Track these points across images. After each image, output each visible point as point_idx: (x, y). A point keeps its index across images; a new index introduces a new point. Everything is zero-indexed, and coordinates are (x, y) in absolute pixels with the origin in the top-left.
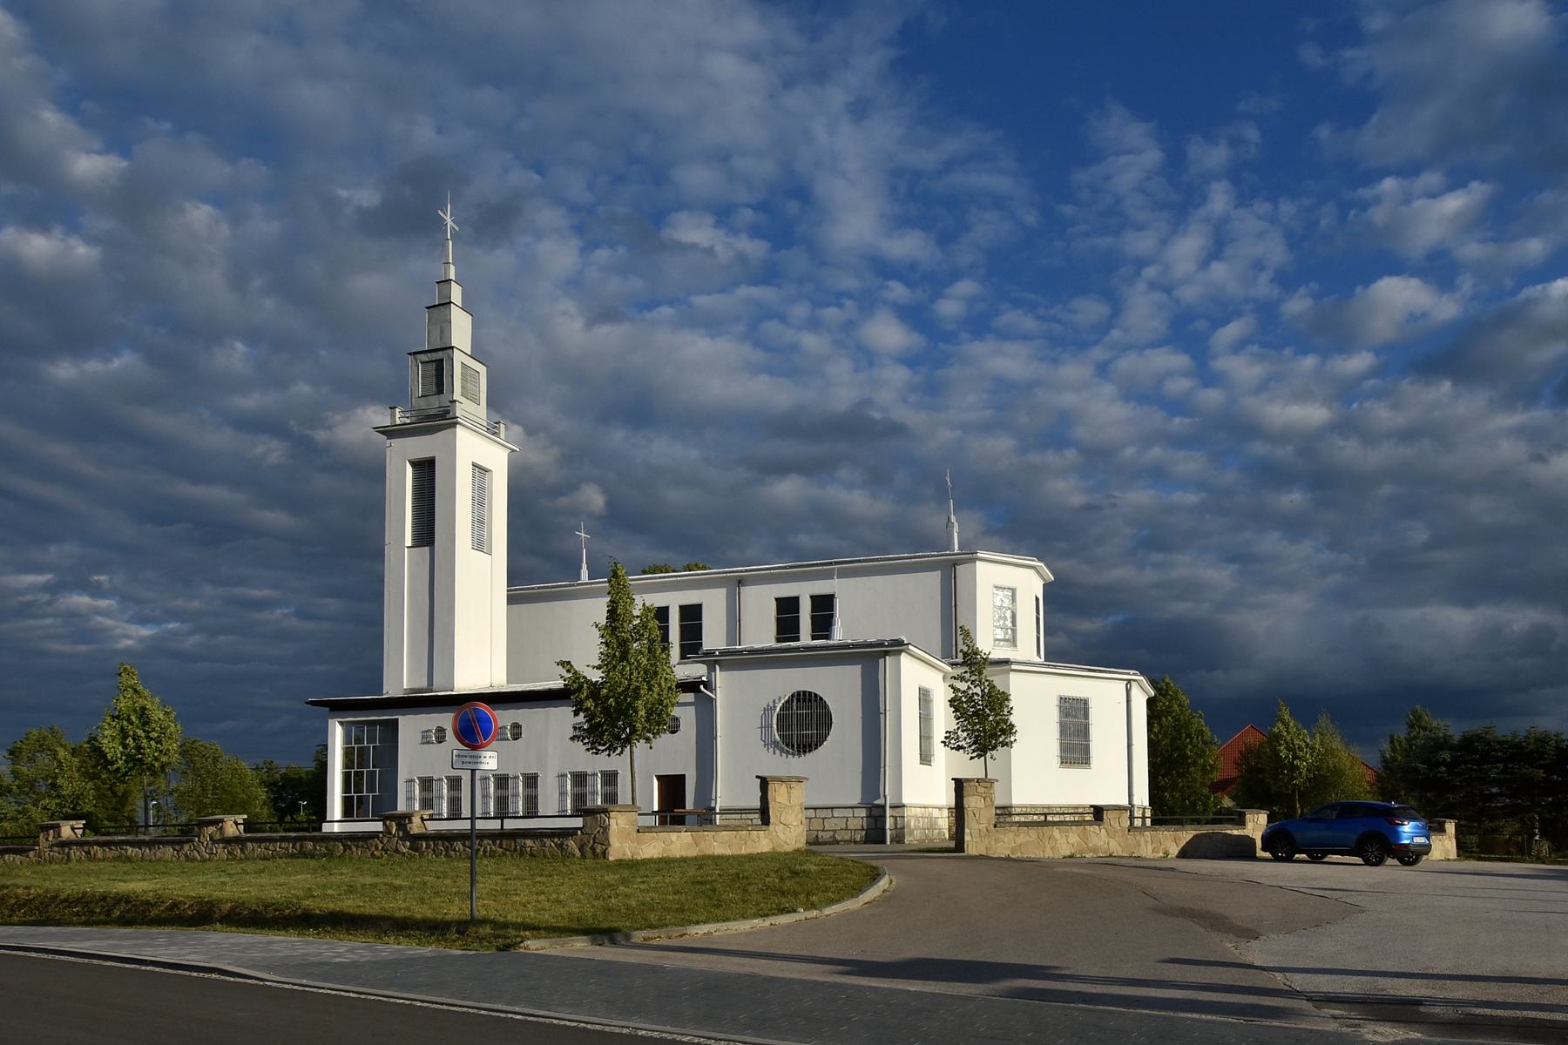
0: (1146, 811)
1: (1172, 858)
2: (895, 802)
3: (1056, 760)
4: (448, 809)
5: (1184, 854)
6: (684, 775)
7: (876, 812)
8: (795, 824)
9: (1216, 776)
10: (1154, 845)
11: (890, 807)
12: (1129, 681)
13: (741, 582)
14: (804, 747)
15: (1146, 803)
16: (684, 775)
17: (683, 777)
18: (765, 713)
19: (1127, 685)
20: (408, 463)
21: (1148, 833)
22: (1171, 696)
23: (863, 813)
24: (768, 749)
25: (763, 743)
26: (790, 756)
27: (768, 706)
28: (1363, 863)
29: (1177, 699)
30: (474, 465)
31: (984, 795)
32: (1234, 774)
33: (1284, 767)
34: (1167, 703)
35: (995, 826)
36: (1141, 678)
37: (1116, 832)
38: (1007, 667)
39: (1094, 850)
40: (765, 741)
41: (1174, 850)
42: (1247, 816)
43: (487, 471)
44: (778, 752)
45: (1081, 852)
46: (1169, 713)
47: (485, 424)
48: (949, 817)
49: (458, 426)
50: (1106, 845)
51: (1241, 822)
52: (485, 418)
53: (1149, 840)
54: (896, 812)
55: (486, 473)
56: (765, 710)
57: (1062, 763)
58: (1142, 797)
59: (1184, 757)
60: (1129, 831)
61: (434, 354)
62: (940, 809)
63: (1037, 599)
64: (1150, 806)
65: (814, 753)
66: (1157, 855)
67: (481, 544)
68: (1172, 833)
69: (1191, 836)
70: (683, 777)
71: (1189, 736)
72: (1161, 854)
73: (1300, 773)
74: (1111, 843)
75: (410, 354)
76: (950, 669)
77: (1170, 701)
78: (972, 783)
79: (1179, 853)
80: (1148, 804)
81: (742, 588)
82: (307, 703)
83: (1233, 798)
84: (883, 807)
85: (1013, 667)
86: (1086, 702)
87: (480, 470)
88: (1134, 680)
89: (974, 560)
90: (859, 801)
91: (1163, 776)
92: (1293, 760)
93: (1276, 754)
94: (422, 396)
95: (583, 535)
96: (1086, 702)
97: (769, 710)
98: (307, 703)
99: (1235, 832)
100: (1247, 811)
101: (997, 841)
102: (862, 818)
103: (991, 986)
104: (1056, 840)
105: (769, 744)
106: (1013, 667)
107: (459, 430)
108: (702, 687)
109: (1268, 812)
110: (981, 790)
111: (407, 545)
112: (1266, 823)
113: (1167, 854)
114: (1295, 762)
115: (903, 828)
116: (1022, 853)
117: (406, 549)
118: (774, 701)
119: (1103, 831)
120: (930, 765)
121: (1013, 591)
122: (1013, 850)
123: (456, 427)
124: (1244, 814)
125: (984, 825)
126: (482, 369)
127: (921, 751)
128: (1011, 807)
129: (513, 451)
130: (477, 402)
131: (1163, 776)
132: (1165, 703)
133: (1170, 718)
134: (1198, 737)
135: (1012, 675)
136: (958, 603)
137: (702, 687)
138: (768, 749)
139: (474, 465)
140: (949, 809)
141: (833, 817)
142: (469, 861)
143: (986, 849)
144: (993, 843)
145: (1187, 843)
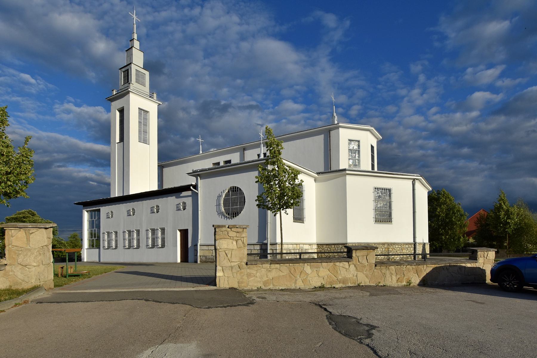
0: (426, 245)
1: (414, 286)
2: (273, 242)
3: (372, 220)
4: (128, 244)
5: (425, 283)
6: (188, 229)
7: (264, 247)
8: (35, 264)
9: (466, 229)
10: (398, 276)
11: (270, 244)
12: (414, 180)
13: (244, 149)
14: (236, 214)
15: (426, 240)
16: (188, 229)
17: (187, 230)
18: (218, 198)
19: (413, 182)
20: (117, 110)
21: (393, 267)
22: (446, 196)
23: (258, 247)
24: (219, 216)
25: (217, 213)
26: (228, 219)
27: (219, 195)
28: (139, 49)
29: (448, 198)
30: (139, 108)
31: (237, 238)
32: (474, 228)
33: (501, 223)
34: (444, 199)
35: (247, 264)
36: (421, 178)
37: (365, 266)
38: (344, 173)
39: (344, 281)
40: (218, 212)
41: (416, 280)
42: (479, 253)
43: (148, 112)
44: (223, 217)
45: (331, 283)
46: (445, 204)
47: (149, 94)
48: (317, 249)
49: (130, 93)
50: (355, 277)
51: (474, 257)
52: (148, 91)
53: (394, 272)
54: (273, 247)
55: (148, 113)
56: (218, 197)
57: (376, 221)
58: (423, 236)
59: (451, 221)
60: (376, 266)
61: (126, 67)
62: (310, 244)
63: (372, 147)
64: (429, 242)
65: (240, 215)
66: (400, 284)
67: (144, 139)
68: (414, 267)
69: (431, 269)
70: (187, 230)
71: (453, 213)
72: (404, 283)
73: (510, 226)
74: (358, 275)
75: (119, 69)
76: (316, 175)
77: (446, 198)
78: (224, 229)
79: (420, 282)
80: (428, 241)
81: (245, 152)
82: (75, 204)
83: (474, 238)
84: (267, 244)
85: (347, 172)
86: (390, 190)
87: (143, 112)
88: (417, 179)
89: (338, 128)
90: (257, 241)
91: (442, 229)
92: (507, 219)
93: (498, 217)
94: (123, 85)
95: (200, 140)
96: (390, 190)
97: (220, 196)
98: (75, 204)
99: (469, 265)
100: (478, 249)
101: (249, 275)
102: (258, 250)
103: (421, 277)
104: (307, 274)
105: (220, 213)
106: (347, 172)
107: (131, 94)
108: (191, 187)
109: (496, 250)
110: (232, 234)
111: (116, 142)
112: (494, 258)
113: (409, 283)
114: (508, 221)
115: (214, 261)
116: (274, 285)
117: (116, 144)
118: (221, 193)
119: (352, 267)
120: (304, 223)
121: (359, 141)
122: (265, 283)
123: (129, 93)
124: (476, 251)
125: (236, 263)
126: (147, 73)
127: (294, 216)
128: (347, 244)
129: (160, 104)
130: (144, 85)
131: (442, 229)
132: (443, 199)
133: (445, 206)
134: (458, 213)
135: (348, 177)
136: (331, 149)
137: (191, 187)
138: (219, 216)
139: (139, 108)
140: (317, 245)
141: (254, 249)
142: (271, 252)
143: (238, 283)
144: (245, 277)
145: (427, 274)
